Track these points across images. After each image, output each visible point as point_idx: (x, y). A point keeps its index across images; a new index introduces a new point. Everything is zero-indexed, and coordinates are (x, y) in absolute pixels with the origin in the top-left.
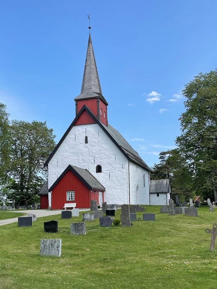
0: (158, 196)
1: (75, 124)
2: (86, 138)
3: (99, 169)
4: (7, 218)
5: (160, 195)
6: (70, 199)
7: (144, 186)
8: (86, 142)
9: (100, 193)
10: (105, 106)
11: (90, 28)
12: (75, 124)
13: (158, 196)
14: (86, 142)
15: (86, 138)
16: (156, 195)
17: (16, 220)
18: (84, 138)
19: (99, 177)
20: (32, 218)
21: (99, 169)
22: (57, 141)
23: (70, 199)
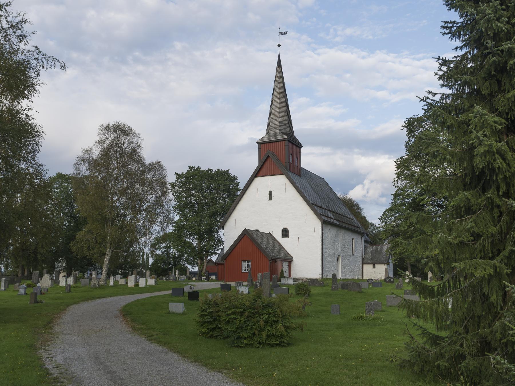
0: (374, 267)
1: (257, 174)
2: (270, 193)
3: (285, 233)
4: (155, 292)
5: (376, 265)
6: (245, 270)
7: (353, 255)
8: (270, 198)
9: (285, 265)
10: (298, 149)
11: (279, 46)
12: (257, 174)
13: (374, 267)
14: (270, 198)
15: (270, 193)
16: (372, 265)
17: (170, 292)
18: (268, 193)
19: (283, 242)
20: (38, 295)
21: (285, 233)
22: (242, 186)
23: (245, 270)
